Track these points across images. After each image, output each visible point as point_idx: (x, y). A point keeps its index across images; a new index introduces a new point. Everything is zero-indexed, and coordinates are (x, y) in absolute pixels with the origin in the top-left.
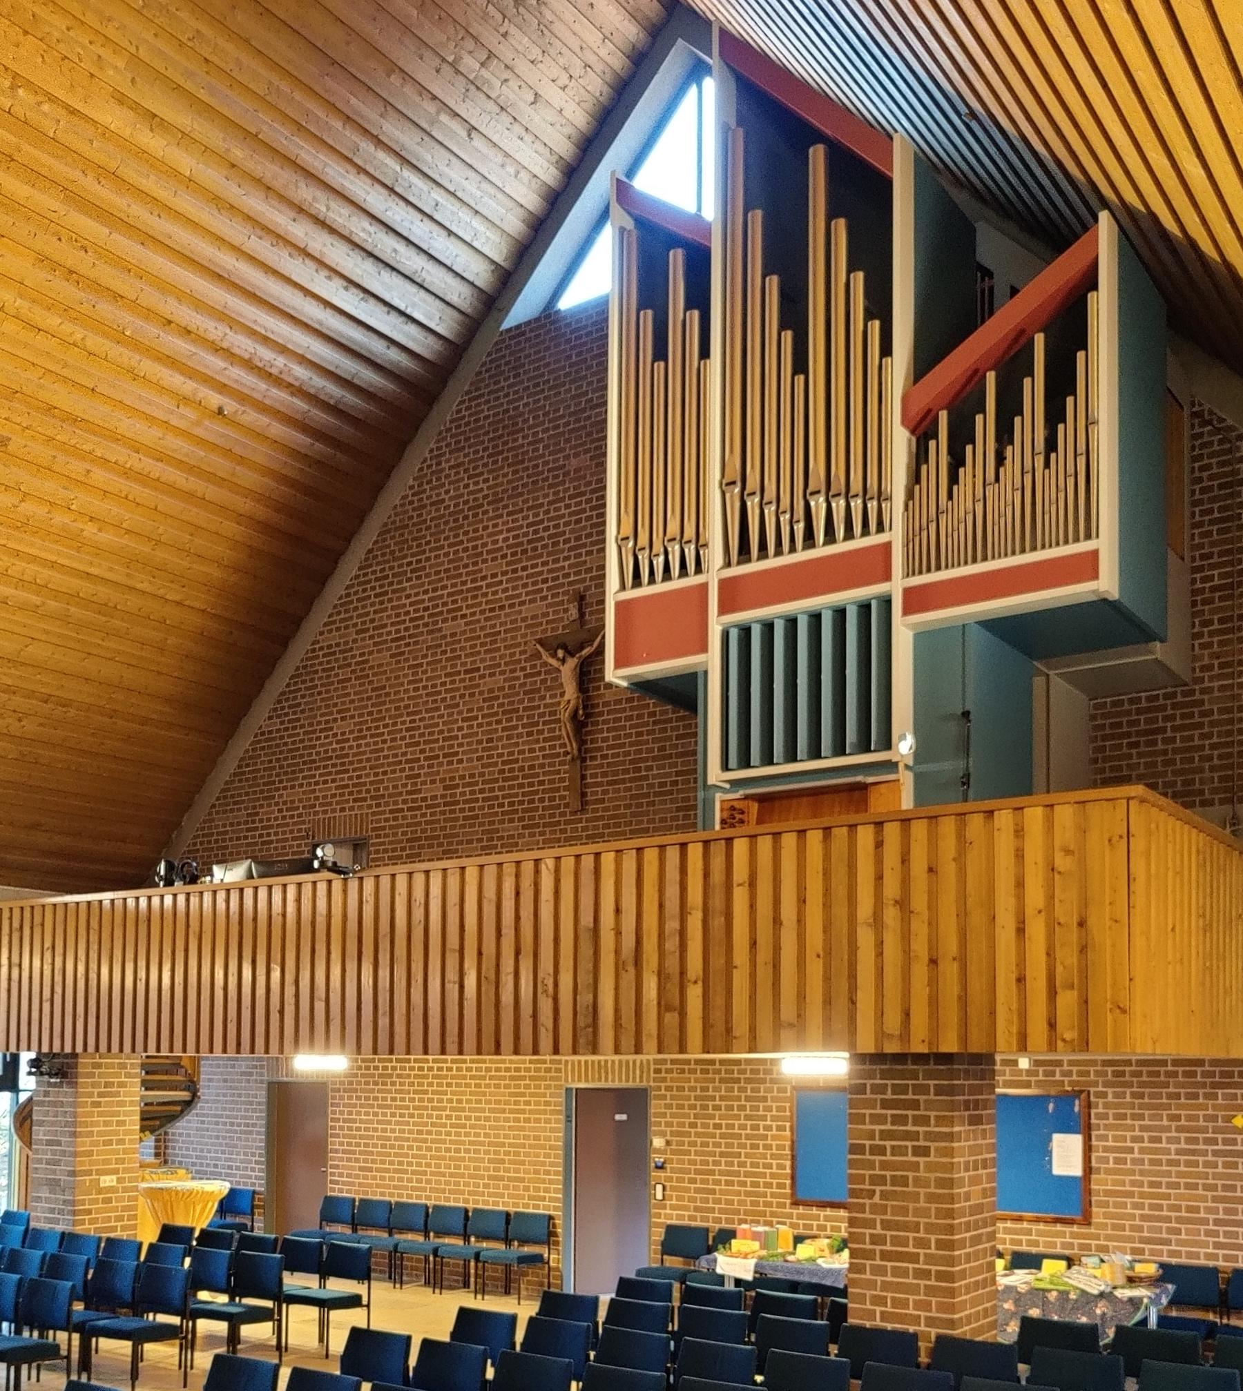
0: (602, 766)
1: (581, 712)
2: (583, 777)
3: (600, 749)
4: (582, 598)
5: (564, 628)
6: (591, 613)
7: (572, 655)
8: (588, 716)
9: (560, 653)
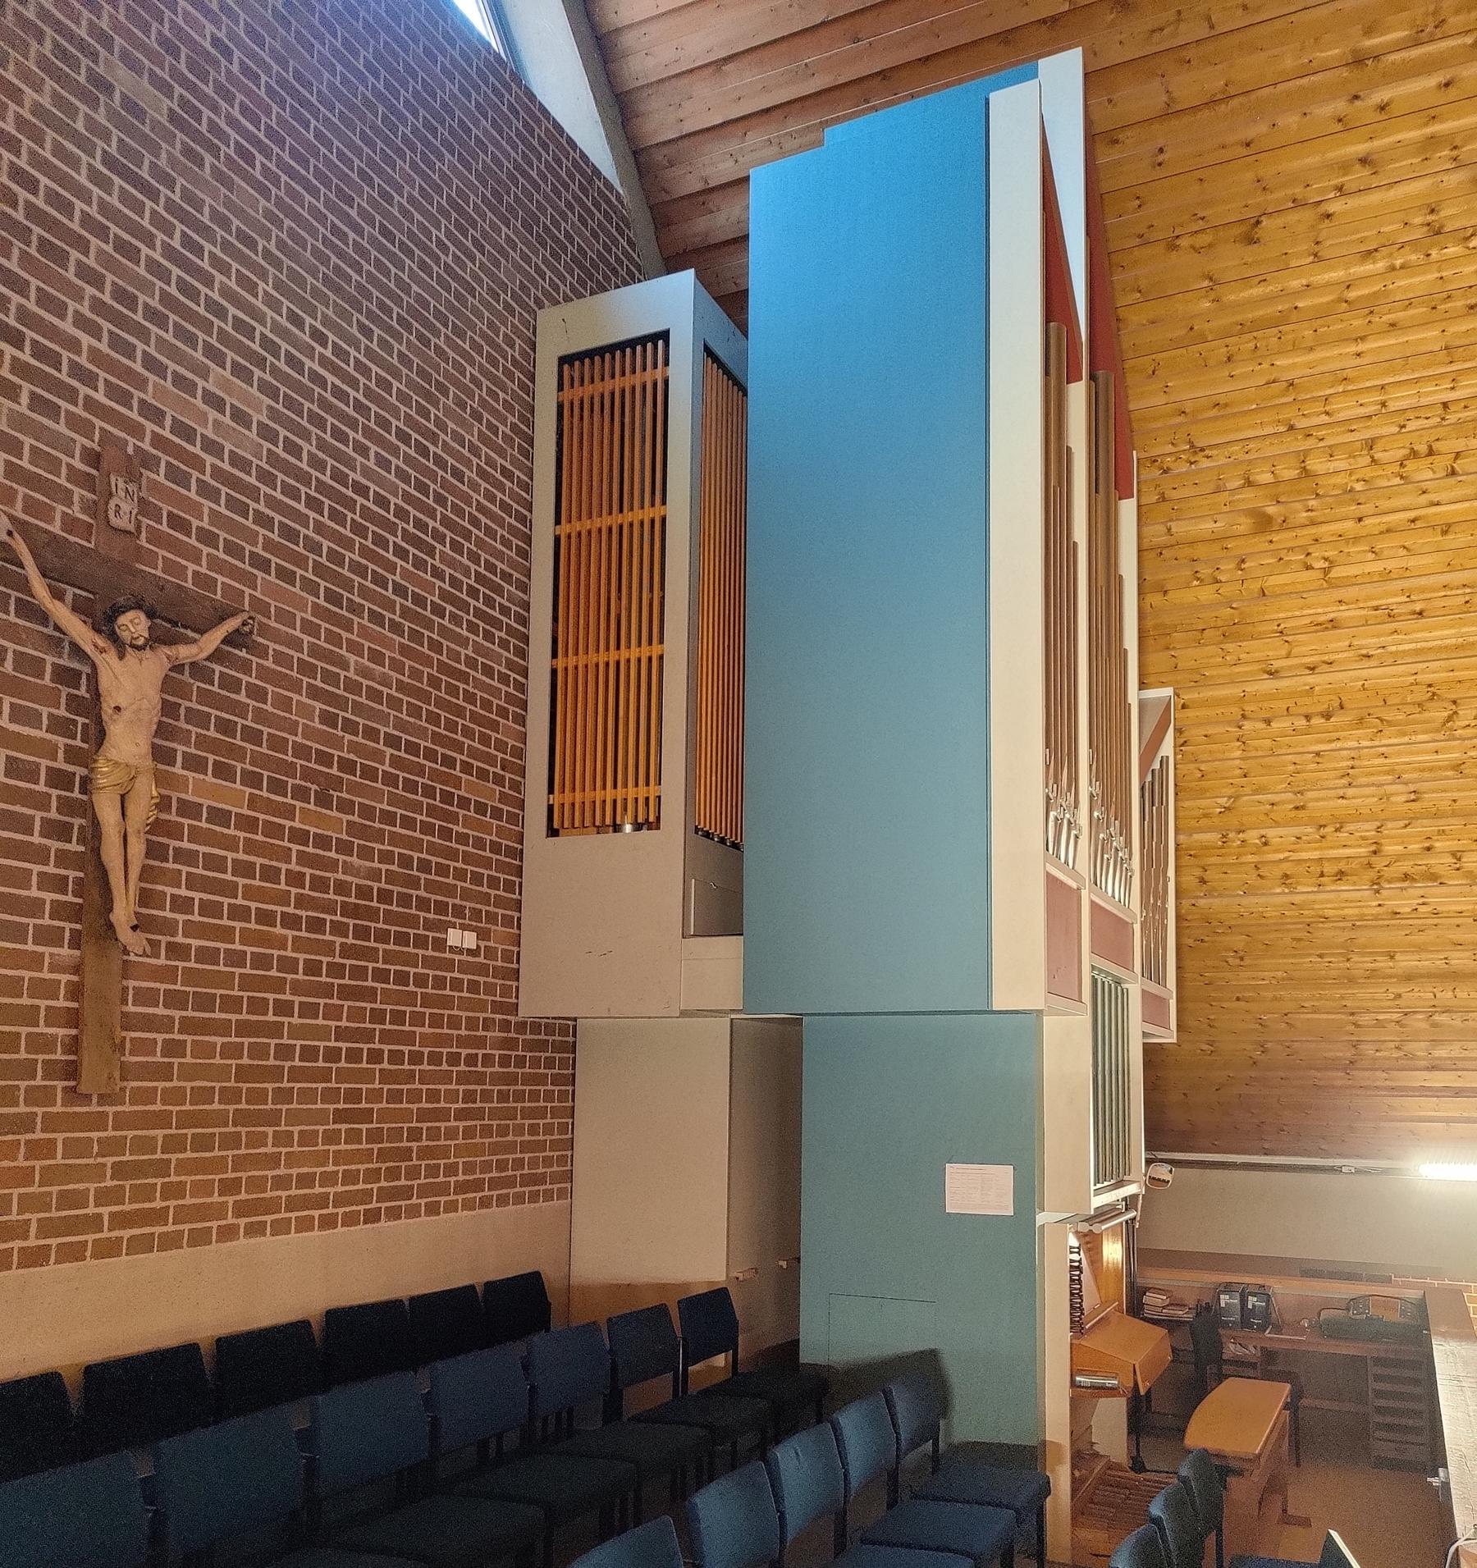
0: (169, 974)
5: (70, 524)
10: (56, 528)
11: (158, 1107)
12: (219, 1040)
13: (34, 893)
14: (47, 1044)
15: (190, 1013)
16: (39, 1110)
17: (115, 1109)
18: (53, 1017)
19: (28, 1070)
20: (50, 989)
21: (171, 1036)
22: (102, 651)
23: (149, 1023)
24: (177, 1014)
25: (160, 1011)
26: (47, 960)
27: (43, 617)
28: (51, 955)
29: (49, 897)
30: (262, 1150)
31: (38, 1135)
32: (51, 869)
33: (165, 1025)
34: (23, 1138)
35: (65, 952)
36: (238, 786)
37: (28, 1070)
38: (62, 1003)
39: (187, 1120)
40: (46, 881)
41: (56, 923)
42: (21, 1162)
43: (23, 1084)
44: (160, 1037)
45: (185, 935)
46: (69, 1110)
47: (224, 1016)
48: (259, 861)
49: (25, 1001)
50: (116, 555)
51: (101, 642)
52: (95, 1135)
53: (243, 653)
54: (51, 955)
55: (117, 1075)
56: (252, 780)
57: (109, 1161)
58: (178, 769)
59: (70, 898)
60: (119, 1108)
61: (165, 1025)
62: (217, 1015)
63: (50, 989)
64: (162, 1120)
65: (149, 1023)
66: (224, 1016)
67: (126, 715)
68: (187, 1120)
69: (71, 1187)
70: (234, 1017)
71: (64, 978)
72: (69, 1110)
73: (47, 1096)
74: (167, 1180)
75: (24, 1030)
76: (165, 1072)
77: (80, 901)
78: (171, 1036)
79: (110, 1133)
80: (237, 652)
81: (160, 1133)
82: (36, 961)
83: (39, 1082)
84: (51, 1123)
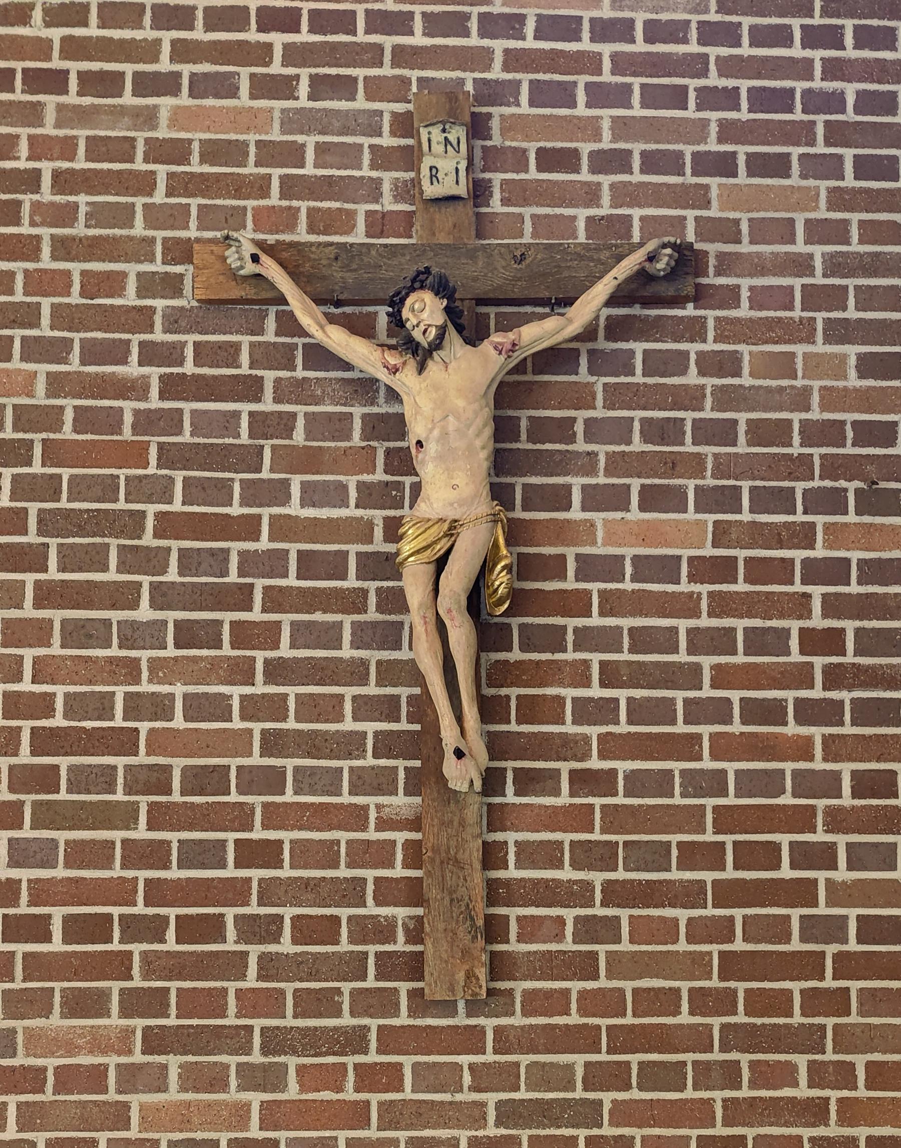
0: (580, 818)
1: (500, 580)
2: (492, 856)
3: (571, 747)
4: (478, 127)
5: (378, 224)
6: (518, 194)
7: (474, 335)
8: (519, 601)
9: (425, 312)
10: (359, 236)
11: (574, 1019)
12: (683, 915)
13: (349, 725)
14: (383, 931)
15: (620, 875)
16: (373, 1023)
17: (496, 1021)
18: (386, 892)
19: (355, 967)
20: (380, 854)
21: (589, 911)
22: (394, 370)
23: (549, 893)
24: (598, 878)
25: (567, 874)
26: (373, 815)
27: (319, 356)
28: (379, 807)
29: (370, 727)
30: (787, 1092)
31: (373, 1057)
32: (372, 689)
33: (580, 894)
34: (350, 1060)
35: (401, 802)
36: (691, 515)
37: (355, 967)
38: (398, 871)
39: (624, 1039)
40: (366, 708)
41: (383, 762)
42: (350, 1094)
43: (347, 987)
44: (569, 914)
45: (602, 756)
46: (419, 1022)
47: (688, 875)
48: (741, 624)
49: (343, 872)
50: (442, 238)
51: (393, 359)
52: (464, 1060)
53: (690, 310)
54: (379, 807)
55: (482, 973)
56: (710, 500)
57: (492, 1098)
58: (576, 513)
59: (403, 725)
60: (504, 1021)
61: (580, 894)
62: (675, 875)
63: (380, 854)
64: (585, 1040)
65: (549, 893)
66: (688, 875)
67: (432, 448)
68: (624, 1039)
69: (427, 1133)
70: (708, 876)
71: (400, 837)
72: (419, 1022)
73: (384, 1003)
74: (595, 1132)
75: (344, 913)
76: (585, 967)
77: (417, 727)
78: (589, 911)
79: (490, 1057)
80: (679, 312)
81: (579, 1060)
82: (356, 818)
83: (371, 983)
84: (390, 1040)
